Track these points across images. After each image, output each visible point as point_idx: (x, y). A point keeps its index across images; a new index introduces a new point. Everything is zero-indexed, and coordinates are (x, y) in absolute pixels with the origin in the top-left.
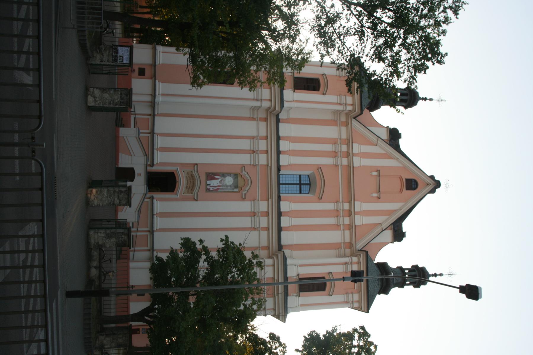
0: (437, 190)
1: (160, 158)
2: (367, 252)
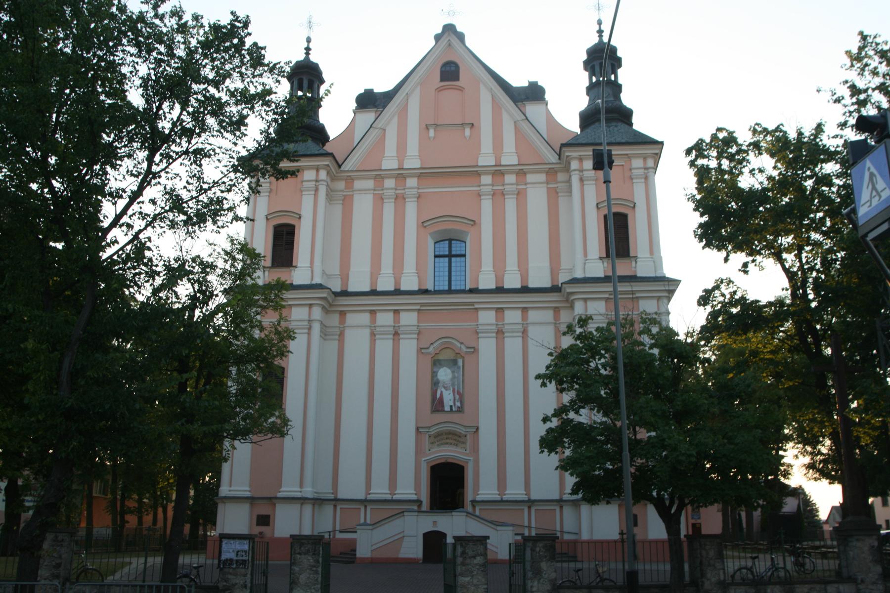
0: (459, 29)
1: (406, 490)
2: (563, 145)
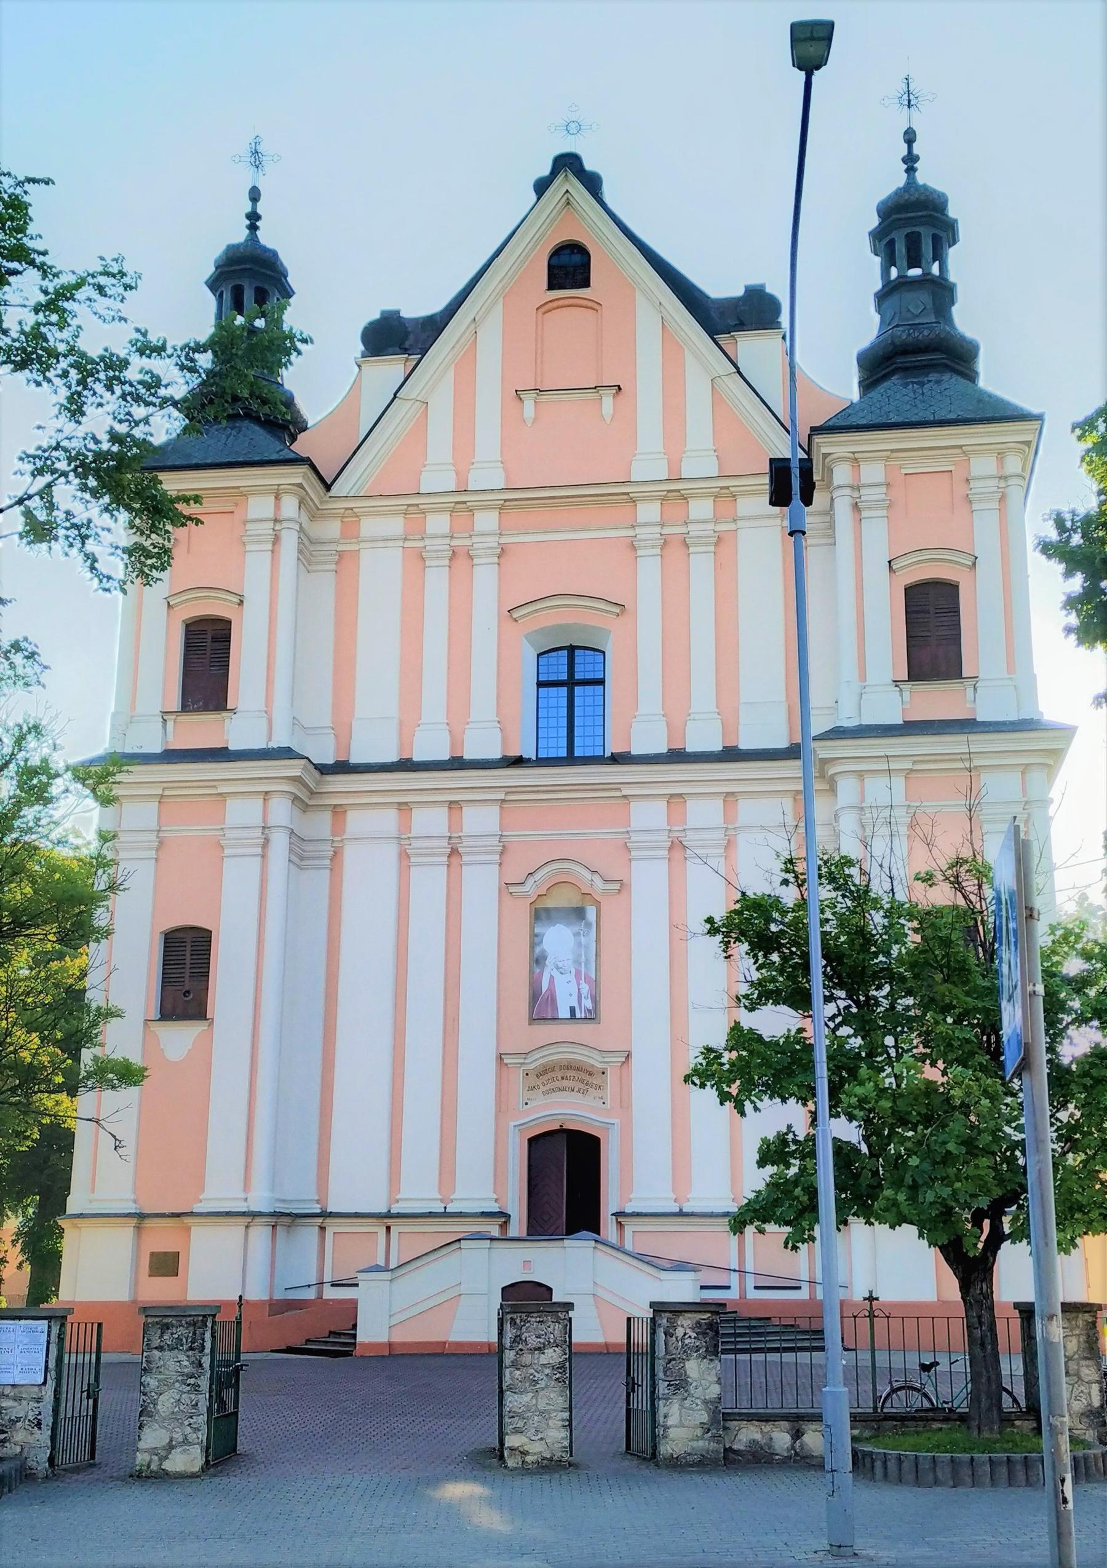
0: (589, 166)
2: (816, 430)
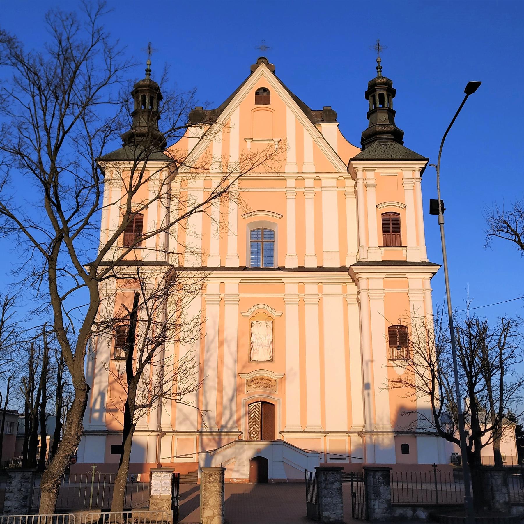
2: (351, 160)
